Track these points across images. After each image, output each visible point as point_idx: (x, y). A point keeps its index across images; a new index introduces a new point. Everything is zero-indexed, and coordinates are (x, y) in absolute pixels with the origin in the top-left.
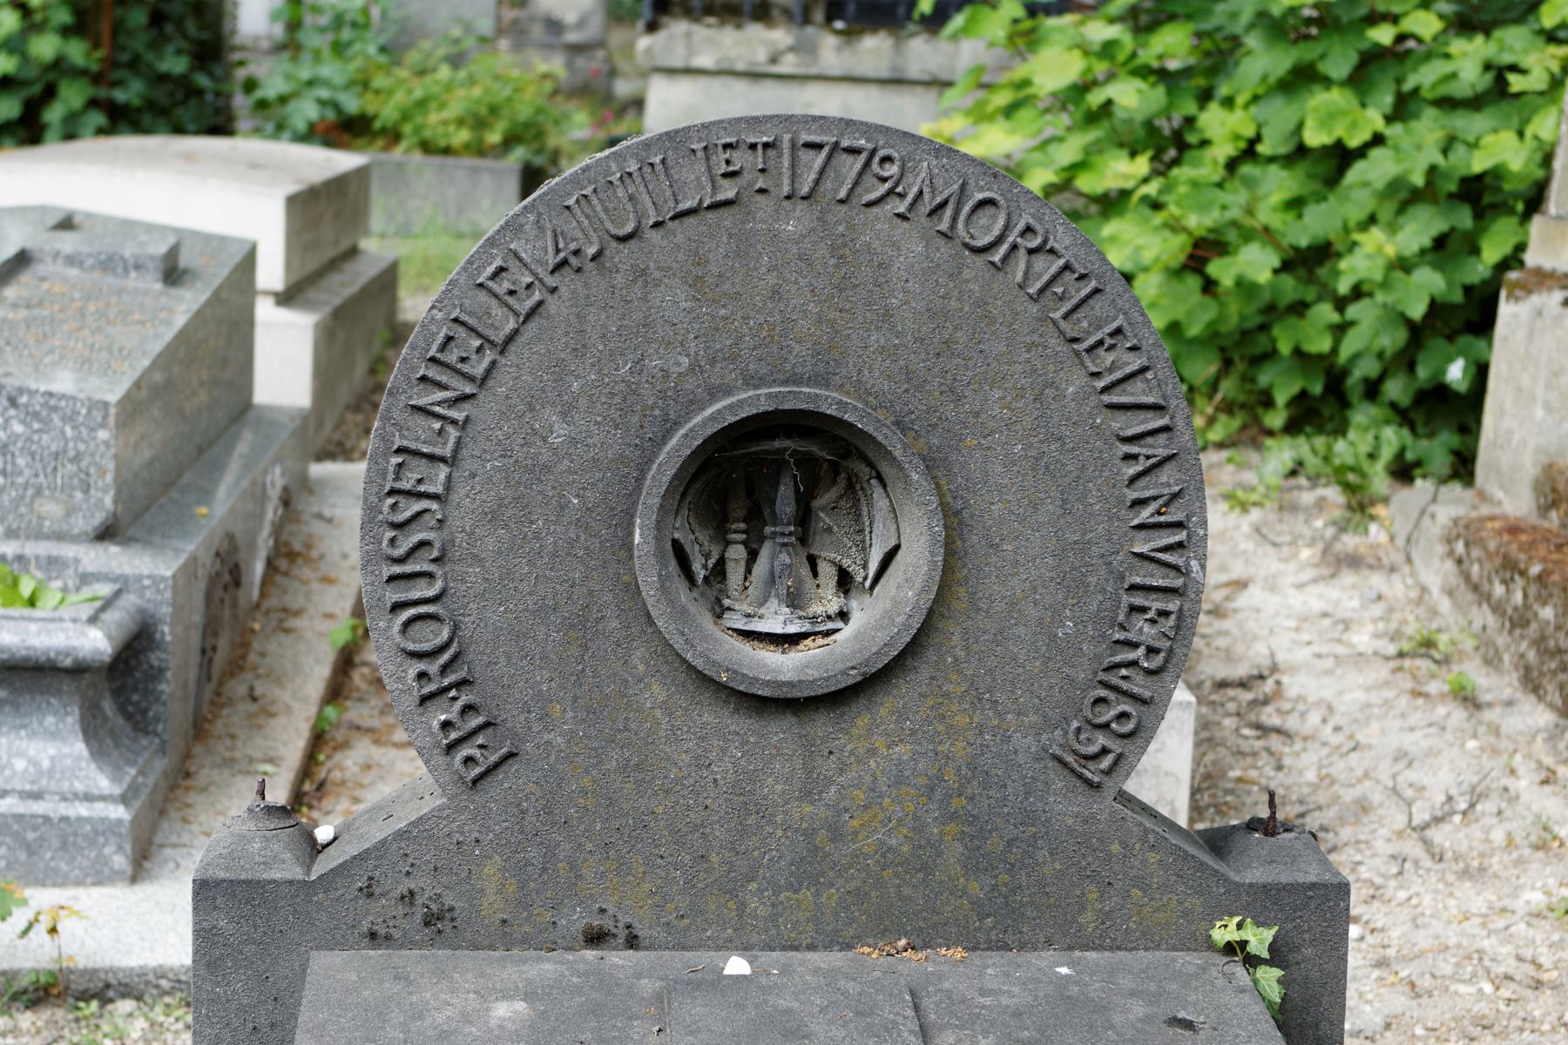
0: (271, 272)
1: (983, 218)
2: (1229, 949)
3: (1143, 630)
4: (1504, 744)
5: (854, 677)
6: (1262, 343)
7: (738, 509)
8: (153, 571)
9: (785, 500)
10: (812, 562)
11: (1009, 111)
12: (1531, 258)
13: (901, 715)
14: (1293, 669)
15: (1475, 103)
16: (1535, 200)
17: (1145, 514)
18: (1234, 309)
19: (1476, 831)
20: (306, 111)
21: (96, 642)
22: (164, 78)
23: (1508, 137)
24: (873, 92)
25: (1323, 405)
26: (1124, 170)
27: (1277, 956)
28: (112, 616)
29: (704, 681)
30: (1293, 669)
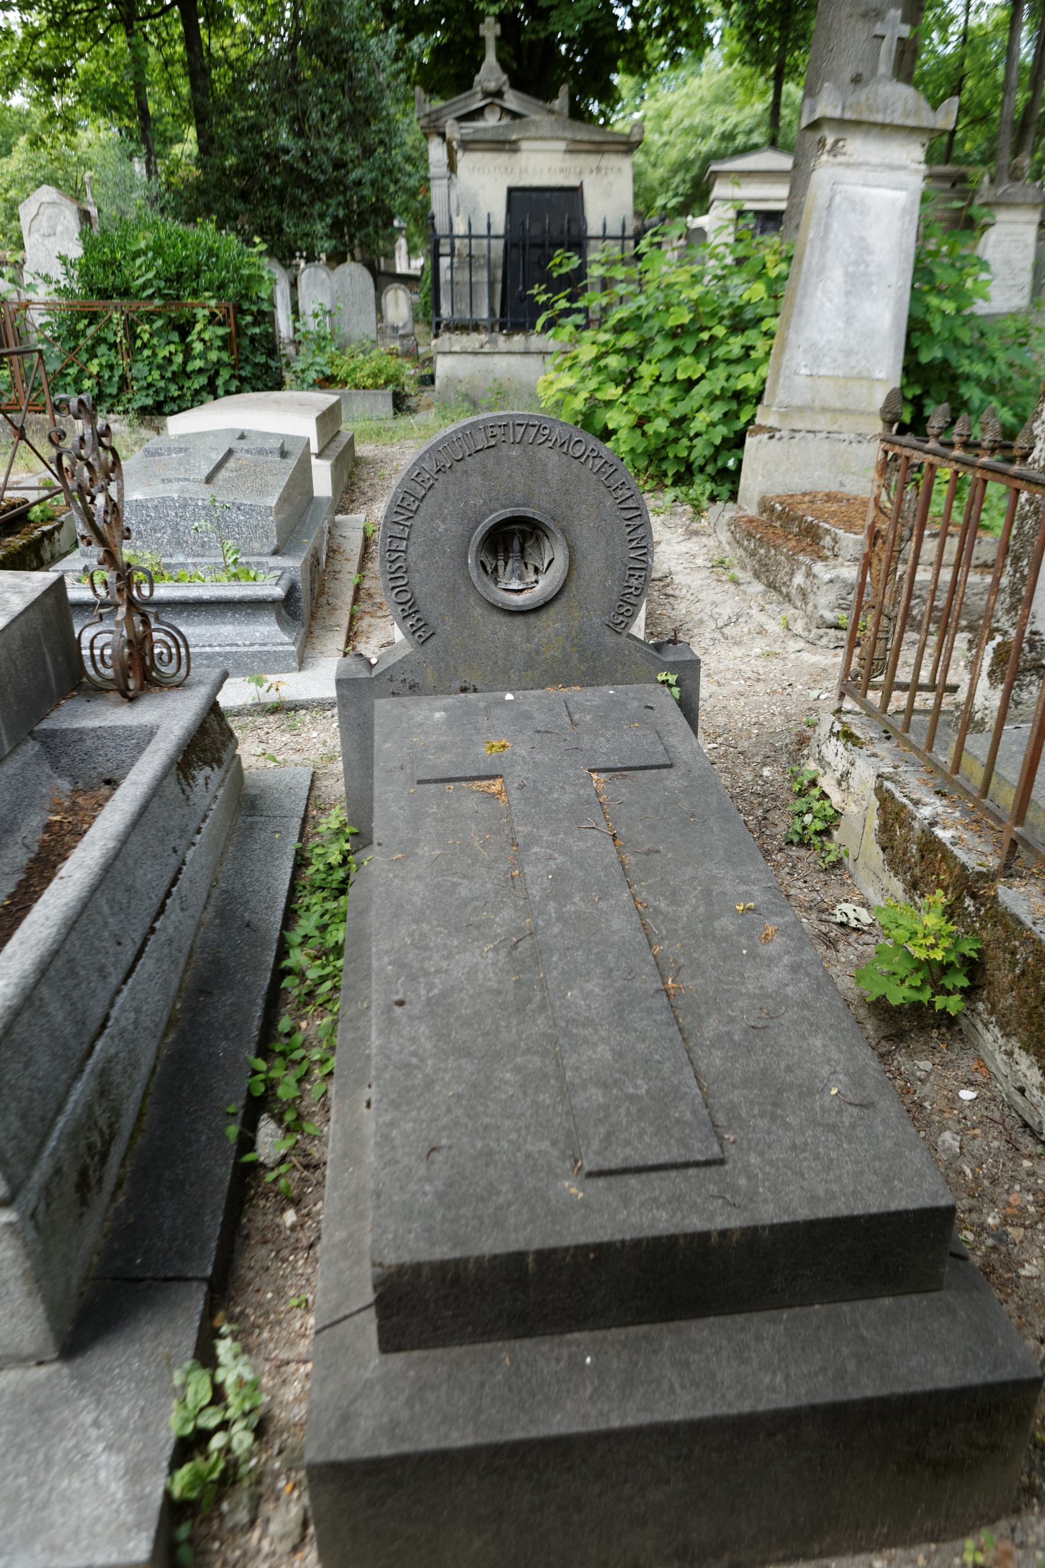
0: (314, 448)
1: (577, 447)
2: (663, 682)
3: (634, 582)
4: (748, 597)
5: (542, 602)
6: (663, 454)
7: (501, 549)
8: (294, 564)
9: (516, 545)
10: (526, 564)
11: (570, 368)
12: (758, 421)
13: (557, 614)
14: (677, 573)
15: (737, 361)
16: (759, 398)
17: (633, 544)
18: (653, 441)
19: (738, 628)
20: (312, 375)
21: (279, 592)
22: (256, 365)
23: (750, 375)
24: (518, 357)
25: (684, 476)
26: (612, 392)
27: (678, 684)
28: (282, 582)
29: (494, 606)
30: (677, 573)
